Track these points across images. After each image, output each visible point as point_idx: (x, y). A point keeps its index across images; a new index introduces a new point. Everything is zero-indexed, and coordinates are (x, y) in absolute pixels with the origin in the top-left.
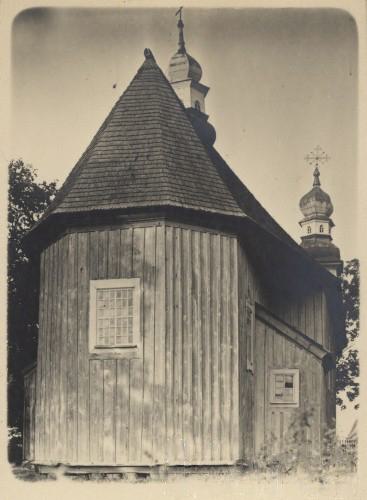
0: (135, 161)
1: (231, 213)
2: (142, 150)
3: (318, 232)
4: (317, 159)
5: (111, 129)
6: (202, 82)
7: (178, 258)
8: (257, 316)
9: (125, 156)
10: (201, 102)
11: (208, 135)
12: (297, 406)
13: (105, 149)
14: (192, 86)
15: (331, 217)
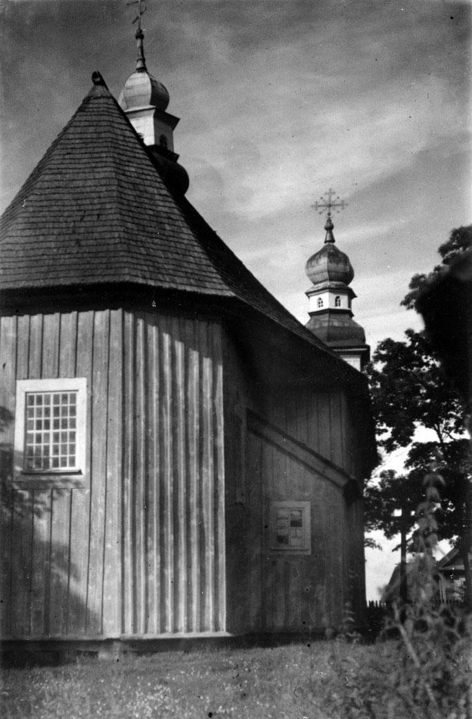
0: (82, 220)
1: (213, 292)
2: (90, 207)
3: (333, 307)
4: (330, 206)
5: (47, 178)
6: (168, 111)
7: (140, 351)
8: (249, 429)
9: (66, 214)
10: (167, 135)
11: (177, 180)
12: (309, 553)
13: (38, 204)
14: (156, 117)
15: (351, 285)
